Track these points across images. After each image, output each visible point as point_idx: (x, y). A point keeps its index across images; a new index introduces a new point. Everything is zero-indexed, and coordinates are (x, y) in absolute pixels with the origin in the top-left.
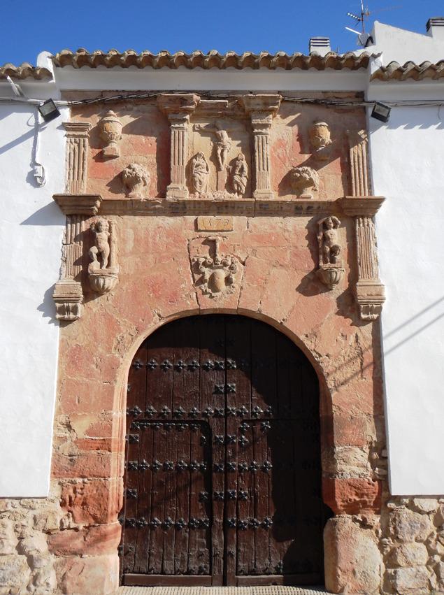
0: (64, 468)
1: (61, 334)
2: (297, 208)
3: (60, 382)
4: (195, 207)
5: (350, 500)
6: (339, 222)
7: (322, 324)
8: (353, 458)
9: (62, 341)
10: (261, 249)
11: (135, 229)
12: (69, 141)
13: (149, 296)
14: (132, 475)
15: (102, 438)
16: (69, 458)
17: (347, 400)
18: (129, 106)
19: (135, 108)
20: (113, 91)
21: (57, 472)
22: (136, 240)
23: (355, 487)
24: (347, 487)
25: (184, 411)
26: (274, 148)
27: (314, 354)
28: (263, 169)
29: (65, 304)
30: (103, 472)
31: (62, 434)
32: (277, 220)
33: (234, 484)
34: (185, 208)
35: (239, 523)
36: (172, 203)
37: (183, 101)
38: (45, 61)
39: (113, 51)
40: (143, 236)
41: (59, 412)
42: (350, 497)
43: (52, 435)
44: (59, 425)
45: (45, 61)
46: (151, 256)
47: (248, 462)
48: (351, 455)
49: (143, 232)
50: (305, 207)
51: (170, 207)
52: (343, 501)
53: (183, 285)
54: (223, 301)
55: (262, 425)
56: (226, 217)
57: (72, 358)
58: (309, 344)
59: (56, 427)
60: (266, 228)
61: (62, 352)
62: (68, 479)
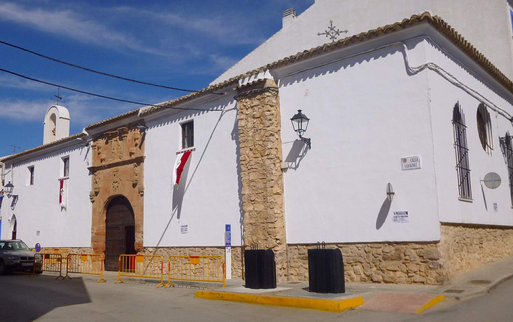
21: (93, 241)
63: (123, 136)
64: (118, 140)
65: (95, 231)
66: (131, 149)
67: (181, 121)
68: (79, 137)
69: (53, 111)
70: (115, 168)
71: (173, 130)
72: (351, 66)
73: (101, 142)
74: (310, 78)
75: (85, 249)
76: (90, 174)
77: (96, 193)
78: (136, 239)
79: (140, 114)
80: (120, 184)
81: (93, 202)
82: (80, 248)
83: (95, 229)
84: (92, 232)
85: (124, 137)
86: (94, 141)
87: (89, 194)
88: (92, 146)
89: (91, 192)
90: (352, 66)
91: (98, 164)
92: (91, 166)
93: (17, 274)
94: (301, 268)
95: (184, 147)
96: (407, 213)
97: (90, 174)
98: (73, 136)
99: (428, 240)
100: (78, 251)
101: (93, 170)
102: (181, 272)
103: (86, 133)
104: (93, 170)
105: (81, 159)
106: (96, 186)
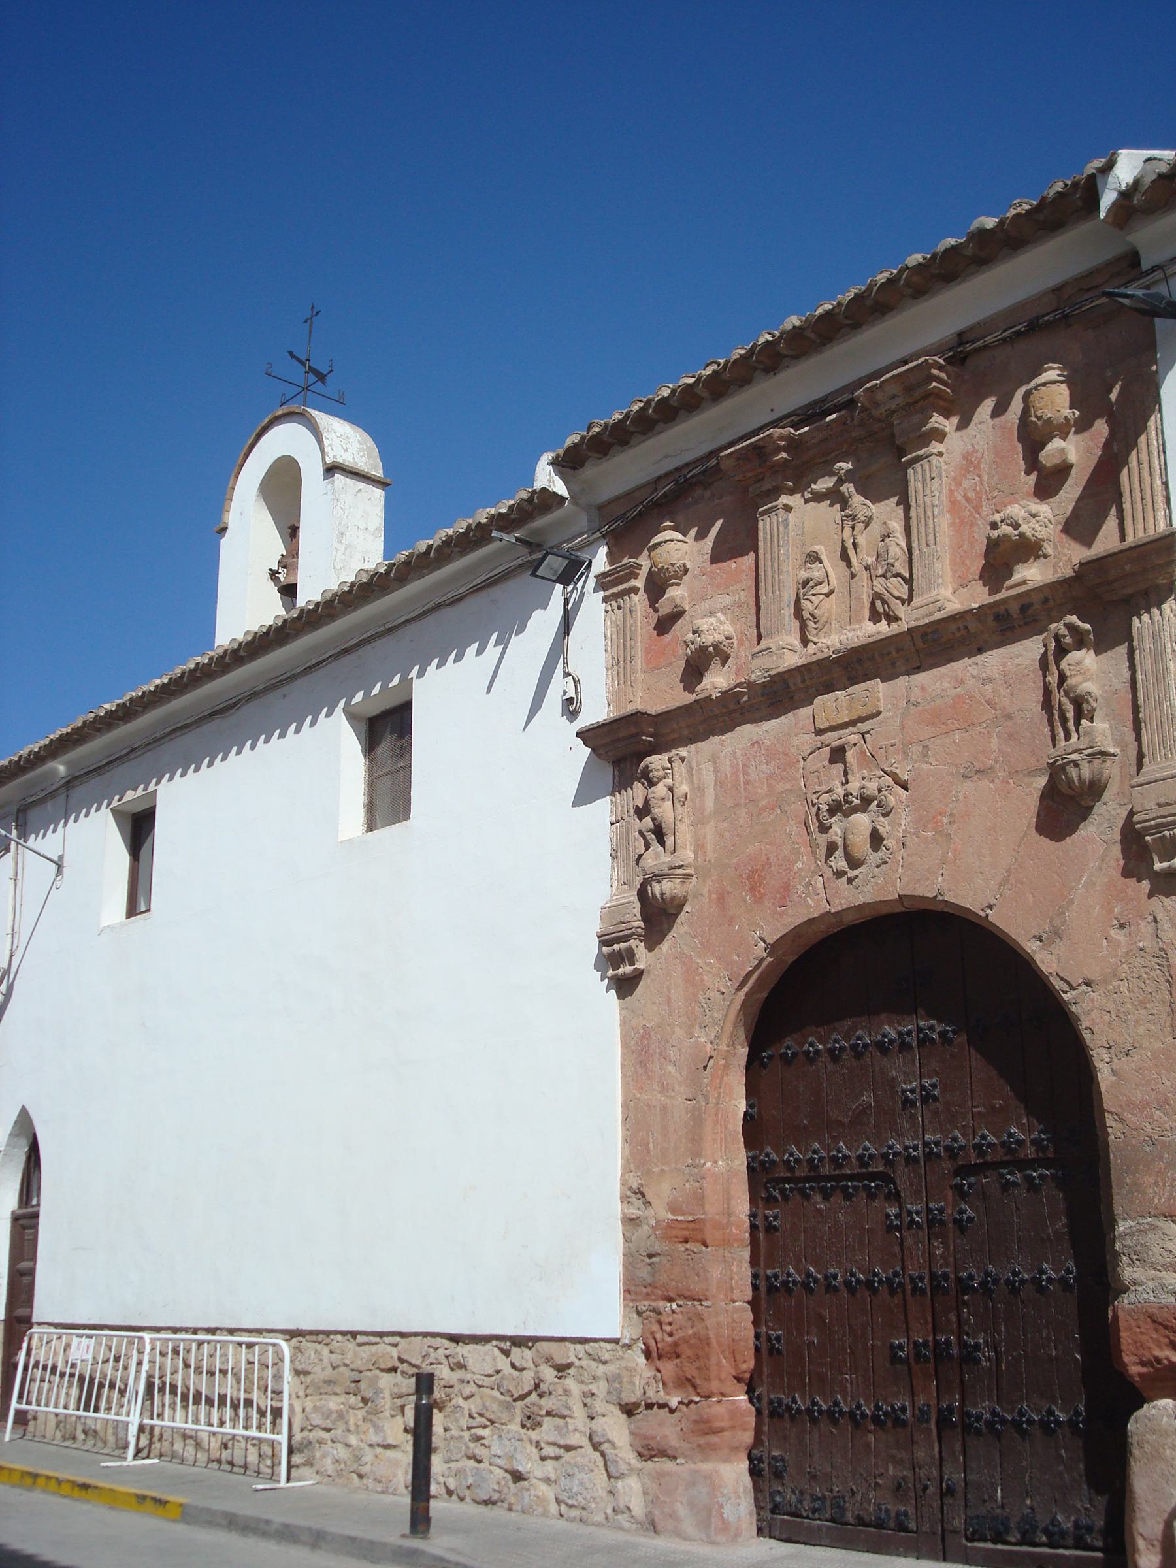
0: (645, 1286)
1: (622, 1009)
2: (998, 618)
3: (625, 1106)
4: (803, 681)
5: (1158, 1360)
6: (1088, 626)
7: (1072, 901)
8: (1156, 1250)
9: (624, 1022)
10: (938, 741)
11: (714, 759)
12: (609, 608)
13: (745, 901)
14: (767, 1296)
15: (690, 1218)
16: (647, 1260)
17: (1139, 1095)
18: (698, 492)
19: (708, 494)
20: (671, 472)
21: (631, 1290)
22: (719, 783)
23: (1166, 1327)
24: (1147, 1325)
25: (848, 1152)
26: (954, 479)
27: (1058, 985)
28: (928, 545)
29: (1167, 833)
30: (696, 1287)
31: (633, 1212)
32: (964, 667)
33: (948, 1321)
34: (788, 687)
35: (965, 1414)
36: (764, 685)
37: (760, 452)
38: (547, 477)
39: (635, 402)
40: (728, 770)
41: (626, 1170)
42: (1157, 1353)
43: (619, 1215)
44: (629, 1193)
45: (547, 477)
46: (744, 811)
47: (978, 1268)
48: (1152, 1239)
49: (728, 763)
50: (1014, 609)
51: (763, 695)
52: (1142, 1363)
53: (799, 865)
54: (877, 886)
55: (1002, 1176)
56: (864, 685)
57: (640, 1053)
58: (1047, 961)
59: (625, 1199)
60: (946, 685)
61: (625, 1045)
62: (647, 1303)
65: (660, 1212)
66: (1016, 511)
69: (285, 440)
70: (832, 705)
73: (678, 546)
75: (571, 1353)
77: (658, 916)
78: (1128, 1273)
79: (1125, 195)
80: (904, 819)
81: (625, 986)
82: (519, 1342)
83: (662, 1192)
84: (630, 1222)
85: (918, 459)
87: (594, 926)
88: (603, 582)
89: (608, 912)
91: (663, 694)
92: (596, 712)
93: (617, 498)
97: (583, 797)
98: (402, 556)
99: (597, 1336)
100: (503, 1363)
101: (622, 751)
103: (560, 487)
105: (505, 714)
106: (656, 859)
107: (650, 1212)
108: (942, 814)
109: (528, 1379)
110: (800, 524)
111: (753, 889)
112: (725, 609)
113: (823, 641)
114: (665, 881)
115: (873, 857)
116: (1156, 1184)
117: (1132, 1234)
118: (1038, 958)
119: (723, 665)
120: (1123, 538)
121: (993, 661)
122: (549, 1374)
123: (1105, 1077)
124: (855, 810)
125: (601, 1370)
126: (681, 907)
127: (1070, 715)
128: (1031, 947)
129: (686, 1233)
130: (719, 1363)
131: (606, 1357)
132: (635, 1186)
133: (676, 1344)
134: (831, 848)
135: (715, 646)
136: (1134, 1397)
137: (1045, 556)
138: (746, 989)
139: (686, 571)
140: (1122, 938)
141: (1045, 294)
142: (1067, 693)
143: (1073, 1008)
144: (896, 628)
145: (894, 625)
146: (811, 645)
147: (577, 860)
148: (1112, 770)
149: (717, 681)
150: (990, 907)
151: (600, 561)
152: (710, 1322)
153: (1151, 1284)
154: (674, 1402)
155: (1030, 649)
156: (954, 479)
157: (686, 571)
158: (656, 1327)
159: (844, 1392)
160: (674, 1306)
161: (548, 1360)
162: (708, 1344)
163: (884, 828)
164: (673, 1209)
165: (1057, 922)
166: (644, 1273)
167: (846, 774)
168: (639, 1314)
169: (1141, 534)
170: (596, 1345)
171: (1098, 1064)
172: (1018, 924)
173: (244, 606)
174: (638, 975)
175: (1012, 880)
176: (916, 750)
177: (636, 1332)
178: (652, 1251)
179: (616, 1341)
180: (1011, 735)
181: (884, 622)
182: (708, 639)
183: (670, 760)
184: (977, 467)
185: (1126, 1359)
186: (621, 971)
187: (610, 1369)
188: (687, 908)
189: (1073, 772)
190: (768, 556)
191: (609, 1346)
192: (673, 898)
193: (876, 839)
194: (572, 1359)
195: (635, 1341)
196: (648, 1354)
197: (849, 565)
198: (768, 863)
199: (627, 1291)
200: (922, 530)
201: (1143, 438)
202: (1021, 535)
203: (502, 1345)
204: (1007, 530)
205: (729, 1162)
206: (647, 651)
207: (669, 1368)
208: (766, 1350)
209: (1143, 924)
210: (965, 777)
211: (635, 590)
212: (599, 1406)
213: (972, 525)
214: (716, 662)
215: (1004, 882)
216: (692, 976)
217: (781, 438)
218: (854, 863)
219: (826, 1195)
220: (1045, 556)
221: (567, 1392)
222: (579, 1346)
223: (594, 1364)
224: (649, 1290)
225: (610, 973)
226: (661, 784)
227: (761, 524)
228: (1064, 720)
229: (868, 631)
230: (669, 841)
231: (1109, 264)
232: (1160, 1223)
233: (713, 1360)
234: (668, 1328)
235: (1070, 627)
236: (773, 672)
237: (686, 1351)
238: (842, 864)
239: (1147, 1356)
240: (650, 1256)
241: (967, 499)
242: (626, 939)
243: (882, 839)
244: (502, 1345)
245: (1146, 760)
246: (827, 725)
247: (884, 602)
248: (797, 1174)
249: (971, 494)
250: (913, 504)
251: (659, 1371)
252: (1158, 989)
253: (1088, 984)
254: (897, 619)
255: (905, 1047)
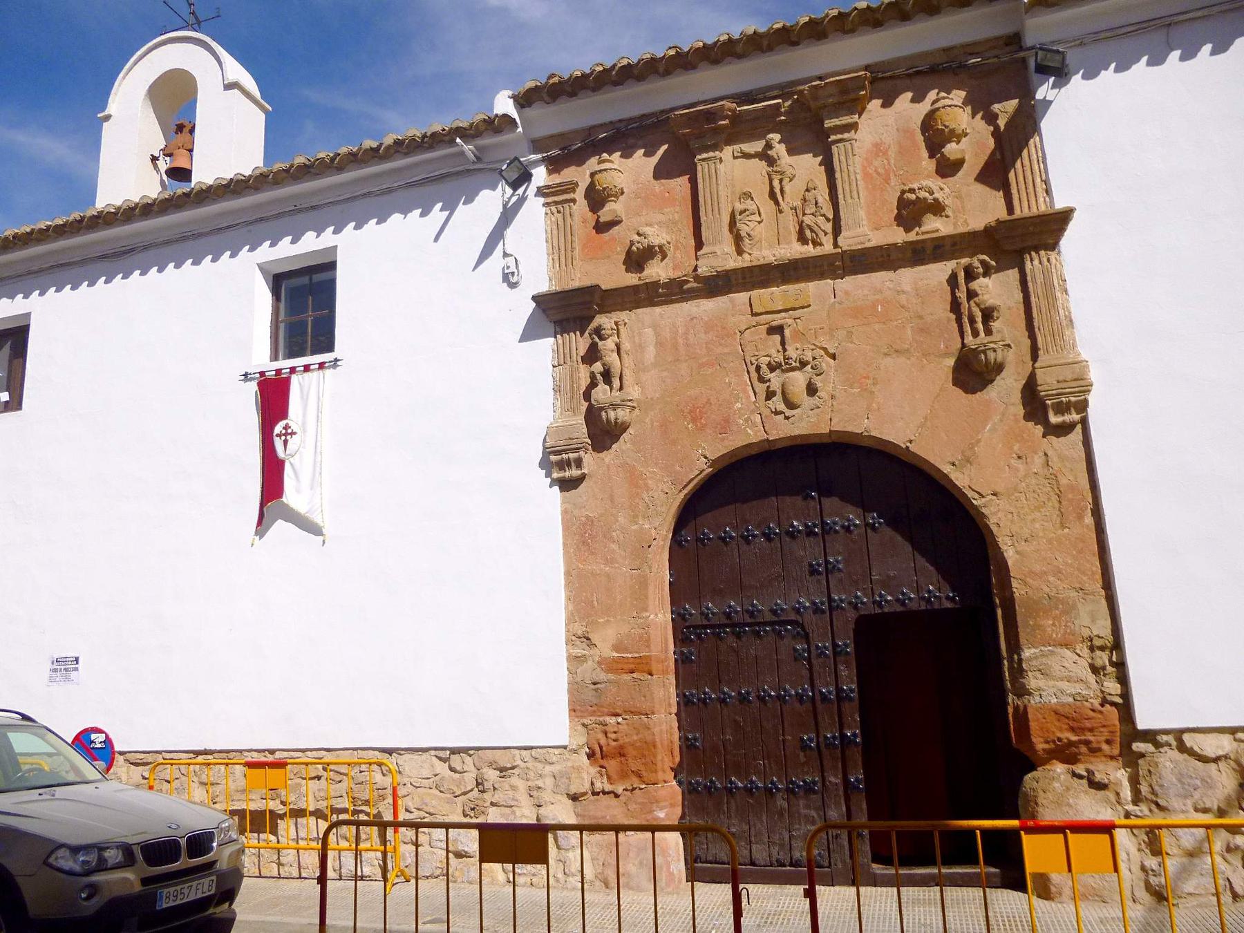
1: (563, 502)
5: (1060, 740)
7: (979, 441)
10: (860, 329)
11: (655, 327)
14: (690, 708)
17: (1037, 568)
21: (575, 710)
22: (660, 344)
26: (866, 159)
27: (970, 494)
30: (645, 706)
31: (577, 652)
37: (710, 116)
38: (504, 105)
41: (570, 621)
42: (1059, 735)
43: (565, 655)
54: (808, 422)
57: (582, 538)
58: (960, 479)
59: (569, 642)
60: (866, 292)
62: (593, 718)
63: (828, 124)
64: (780, 149)
67: (266, 253)
68: (466, 133)
70: (773, 296)
71: (229, 295)
72: (72, 289)
73: (629, 172)
74: (193, 264)
76: (529, 334)
81: (567, 485)
84: (575, 661)
86: (554, 165)
90: (177, 266)
94: (375, 767)
95: (275, 357)
96: (77, 660)
97: (529, 334)
98: (279, 166)
100: (442, 768)
102: (1130, 807)
104: (565, 312)
107: (595, 651)
108: (867, 378)
109: (469, 779)
110: (731, 171)
111: (694, 420)
112: (660, 223)
113: (756, 253)
114: (619, 410)
115: (807, 401)
116: (1054, 624)
117: (1036, 658)
118: (953, 477)
119: (662, 260)
120: (1010, 210)
121: (907, 277)
122: (492, 775)
123: (1010, 555)
124: (793, 369)
125: (548, 768)
126: (625, 430)
127: (979, 319)
128: (946, 469)
129: (632, 666)
130: (662, 760)
131: (554, 759)
132: (580, 633)
133: (621, 747)
134: (770, 395)
135: (660, 247)
136: (1030, 764)
137: (947, 217)
138: (685, 491)
139: (622, 193)
140: (1020, 466)
141: (938, 50)
142: (978, 305)
143: (983, 510)
144: (818, 251)
145: (818, 248)
146: (746, 256)
147: (529, 387)
148: (1010, 357)
149: (657, 271)
150: (911, 442)
151: (540, 176)
152: (656, 730)
153: (1052, 691)
154: (620, 790)
155: (938, 272)
156: (866, 159)
157: (622, 193)
158: (601, 736)
159: (757, 773)
160: (620, 719)
161: (490, 765)
162: (655, 746)
163: (818, 382)
164: (616, 648)
165: (968, 453)
166: (589, 695)
167: (783, 343)
168: (584, 725)
169: (1026, 209)
170: (544, 751)
171: (1004, 548)
172: (938, 453)
173: (125, 171)
174: (582, 478)
175: (928, 423)
176: (842, 334)
177: (582, 740)
178: (597, 680)
179: (565, 747)
180: (922, 330)
181: (811, 245)
182: (656, 241)
183: (616, 323)
184: (885, 153)
185: (1034, 740)
186: (567, 474)
187: (555, 768)
188: (631, 430)
189: (991, 355)
190: (708, 190)
191: (557, 751)
192: (623, 423)
193: (812, 390)
194: (519, 762)
195: (582, 747)
196: (591, 756)
197: (777, 203)
198: (708, 402)
199: (573, 710)
200: (847, 188)
201: (1025, 151)
202: (936, 200)
203: (441, 754)
204: (923, 194)
205: (661, 617)
206: (584, 246)
207: (612, 765)
208: (687, 746)
209: (1036, 457)
210: (886, 354)
211: (574, 201)
212: (546, 796)
213: (882, 190)
214: (659, 257)
215: (922, 426)
216: (635, 480)
217: (729, 110)
218: (791, 405)
219: (738, 636)
220: (947, 217)
221: (514, 788)
222: (524, 753)
223: (540, 766)
224: (595, 708)
225: (555, 475)
226: (609, 340)
227: (699, 168)
228: (972, 321)
229: (796, 250)
230: (616, 383)
231: (988, 40)
232: (1058, 650)
233: (659, 758)
234: (613, 736)
235: (983, 262)
236: (719, 269)
237: (631, 751)
238: (781, 407)
239: (1052, 737)
240: (594, 684)
241: (878, 174)
242: (577, 450)
243: (816, 391)
244: (441, 754)
245: (1041, 353)
246: (762, 310)
247: (812, 231)
248: (713, 622)
249: (881, 171)
250: (837, 168)
251: (602, 767)
252: (1049, 499)
253: (994, 494)
254: (821, 244)
255: (810, 533)
